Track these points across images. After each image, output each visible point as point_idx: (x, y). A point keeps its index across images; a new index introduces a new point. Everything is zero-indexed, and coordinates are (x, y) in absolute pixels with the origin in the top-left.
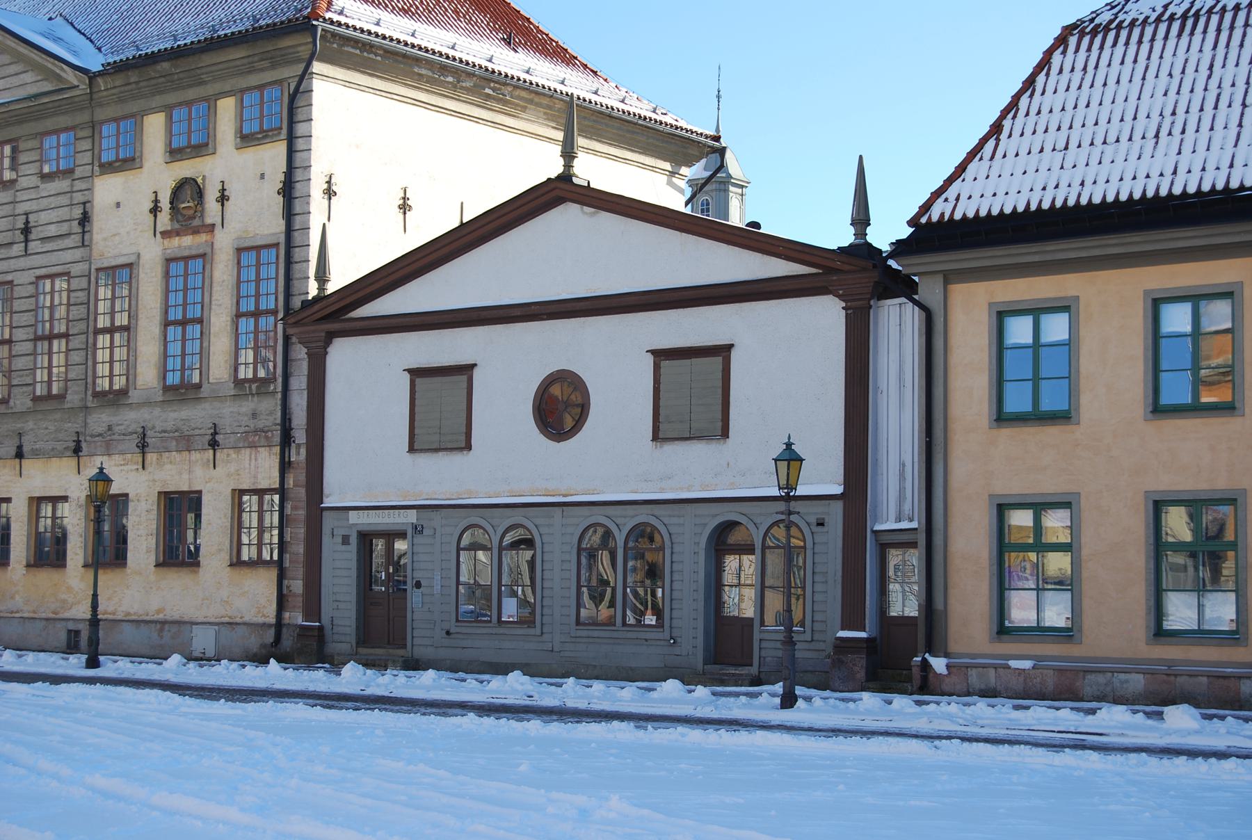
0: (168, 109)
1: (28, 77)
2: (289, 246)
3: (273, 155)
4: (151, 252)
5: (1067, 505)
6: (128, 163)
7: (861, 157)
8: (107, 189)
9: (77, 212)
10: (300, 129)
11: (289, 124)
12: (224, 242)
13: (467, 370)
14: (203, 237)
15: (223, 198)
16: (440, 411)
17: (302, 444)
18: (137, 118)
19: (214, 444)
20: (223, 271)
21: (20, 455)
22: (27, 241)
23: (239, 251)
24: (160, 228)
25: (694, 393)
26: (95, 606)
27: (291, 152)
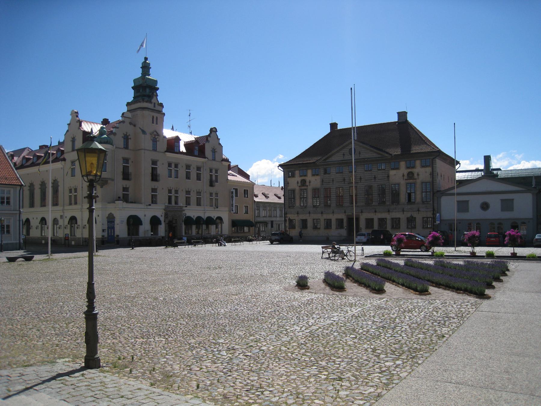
0: (406, 161)
1: (375, 154)
2: (433, 183)
3: (429, 170)
4: (297, 189)
5: (249, 231)
6: (398, 169)
7: (275, 195)
8: (392, 173)
10: (434, 166)
11: (432, 165)
12: (419, 181)
13: (513, 200)
14: (414, 181)
15: (310, 182)
16: (463, 206)
17: (436, 210)
18: (307, 170)
19: (298, 214)
20: (418, 185)
21: (376, 212)
23: (422, 183)
25: (507, 205)
27: (433, 169)
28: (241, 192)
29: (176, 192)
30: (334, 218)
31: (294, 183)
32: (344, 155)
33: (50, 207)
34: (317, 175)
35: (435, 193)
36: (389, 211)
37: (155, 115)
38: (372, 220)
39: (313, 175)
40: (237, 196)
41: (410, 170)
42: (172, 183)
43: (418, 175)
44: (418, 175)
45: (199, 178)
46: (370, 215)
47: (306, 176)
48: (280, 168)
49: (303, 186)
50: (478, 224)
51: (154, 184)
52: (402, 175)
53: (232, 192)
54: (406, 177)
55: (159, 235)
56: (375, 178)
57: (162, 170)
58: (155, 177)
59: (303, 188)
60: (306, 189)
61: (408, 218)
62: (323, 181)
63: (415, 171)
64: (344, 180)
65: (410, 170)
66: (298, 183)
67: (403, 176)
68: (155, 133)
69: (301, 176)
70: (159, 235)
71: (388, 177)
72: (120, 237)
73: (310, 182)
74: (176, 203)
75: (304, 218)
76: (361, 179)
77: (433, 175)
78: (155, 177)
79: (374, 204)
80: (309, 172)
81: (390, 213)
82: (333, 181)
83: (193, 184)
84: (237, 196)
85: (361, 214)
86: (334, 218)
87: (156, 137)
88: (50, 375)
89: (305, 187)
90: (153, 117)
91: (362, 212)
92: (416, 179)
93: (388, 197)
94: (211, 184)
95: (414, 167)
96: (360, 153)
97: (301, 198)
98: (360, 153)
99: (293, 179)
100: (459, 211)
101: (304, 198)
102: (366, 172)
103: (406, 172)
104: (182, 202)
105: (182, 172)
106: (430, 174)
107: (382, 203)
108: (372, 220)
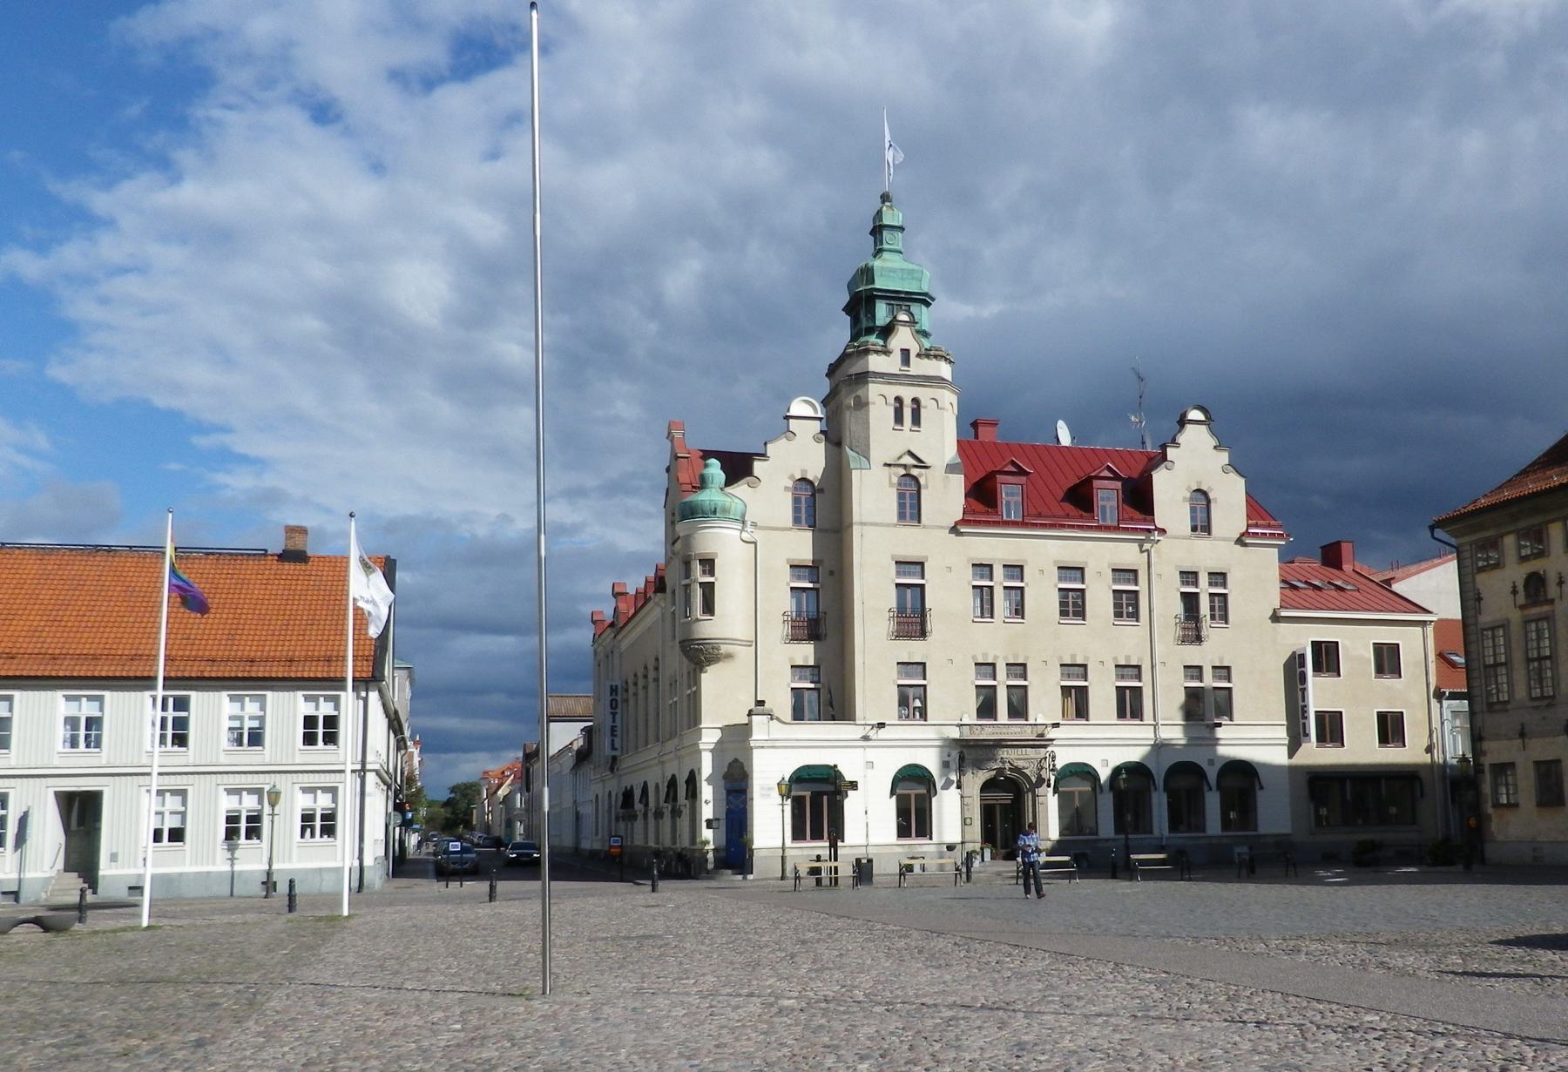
15: (1561, 583)
19: (1522, 735)
29: (1019, 669)
37: (908, 393)
42: (997, 640)
45: (1127, 606)
47: (1541, 554)
48: (1439, 533)
49: (1535, 604)
51: (912, 650)
57: (948, 595)
58: (912, 618)
59: (1535, 611)
61: (858, 861)
66: (1515, 592)
68: (908, 460)
72: (1259, 793)
73: (1561, 583)
74: (1018, 709)
78: (912, 618)
83: (1102, 642)
87: (915, 472)
88: (1521, 981)
89: (1546, 608)
90: (899, 400)
92: (1552, 602)
94: (1192, 630)
97: (1529, 660)
99: (1496, 573)
101: (1540, 659)
104: (1045, 704)
105: (1043, 594)
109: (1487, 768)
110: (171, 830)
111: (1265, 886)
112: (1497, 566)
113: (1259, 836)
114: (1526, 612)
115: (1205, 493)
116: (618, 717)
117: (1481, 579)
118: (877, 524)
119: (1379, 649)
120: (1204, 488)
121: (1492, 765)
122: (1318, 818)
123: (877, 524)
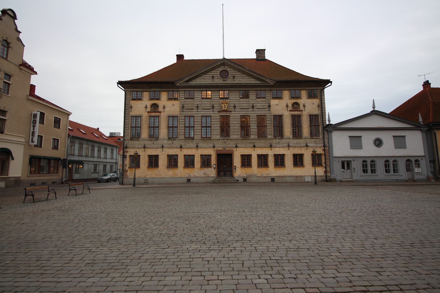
1: (252, 80)
3: (316, 101)
6: (280, 98)
8: (274, 102)
9: (268, 105)
14: (300, 112)
15: (164, 108)
19: (144, 147)
22: (253, 108)
24: (289, 110)
26: (315, 173)
28: (50, 117)
30: (197, 154)
31: (141, 107)
32: (213, 77)
33: (253, 115)
34: (176, 99)
35: (321, 127)
36: (271, 146)
38: (249, 156)
39: (170, 99)
40: (42, 122)
41: (294, 101)
43: (304, 106)
44: (304, 106)
46: (246, 151)
47: (159, 99)
48: (119, 85)
49: (154, 112)
50: (152, 166)
52: (285, 106)
53: (35, 116)
54: (290, 108)
55: (10, 175)
56: (253, 107)
60: (158, 116)
62: (183, 107)
63: (301, 102)
64: (213, 107)
65: (294, 101)
67: (287, 106)
69: (151, 99)
70: (10, 175)
71: (269, 106)
75: (299, 152)
76: (235, 107)
77: (322, 108)
79: (252, 137)
80: (304, 93)
81: (199, 149)
82: (197, 107)
84: (42, 122)
85: (235, 149)
86: (197, 154)
89: (157, 114)
91: (236, 147)
92: (160, 112)
93: (270, 130)
95: (299, 98)
96: (234, 77)
97: (131, 127)
98: (234, 77)
99: (139, 102)
100: (352, 147)
102: (241, 100)
103: (290, 102)
106: (318, 106)
107: (262, 135)
108: (249, 156)
109: (128, 157)
110: (352, 147)
111: (292, 160)
112: (140, 99)
113: (9, 178)
114: (149, 114)
115: (8, 43)
116: (32, 130)
117: (133, 103)
118: (13, 64)
119: (404, 147)
120: (9, 41)
121: (130, 156)
122: (31, 172)
123: (13, 64)
